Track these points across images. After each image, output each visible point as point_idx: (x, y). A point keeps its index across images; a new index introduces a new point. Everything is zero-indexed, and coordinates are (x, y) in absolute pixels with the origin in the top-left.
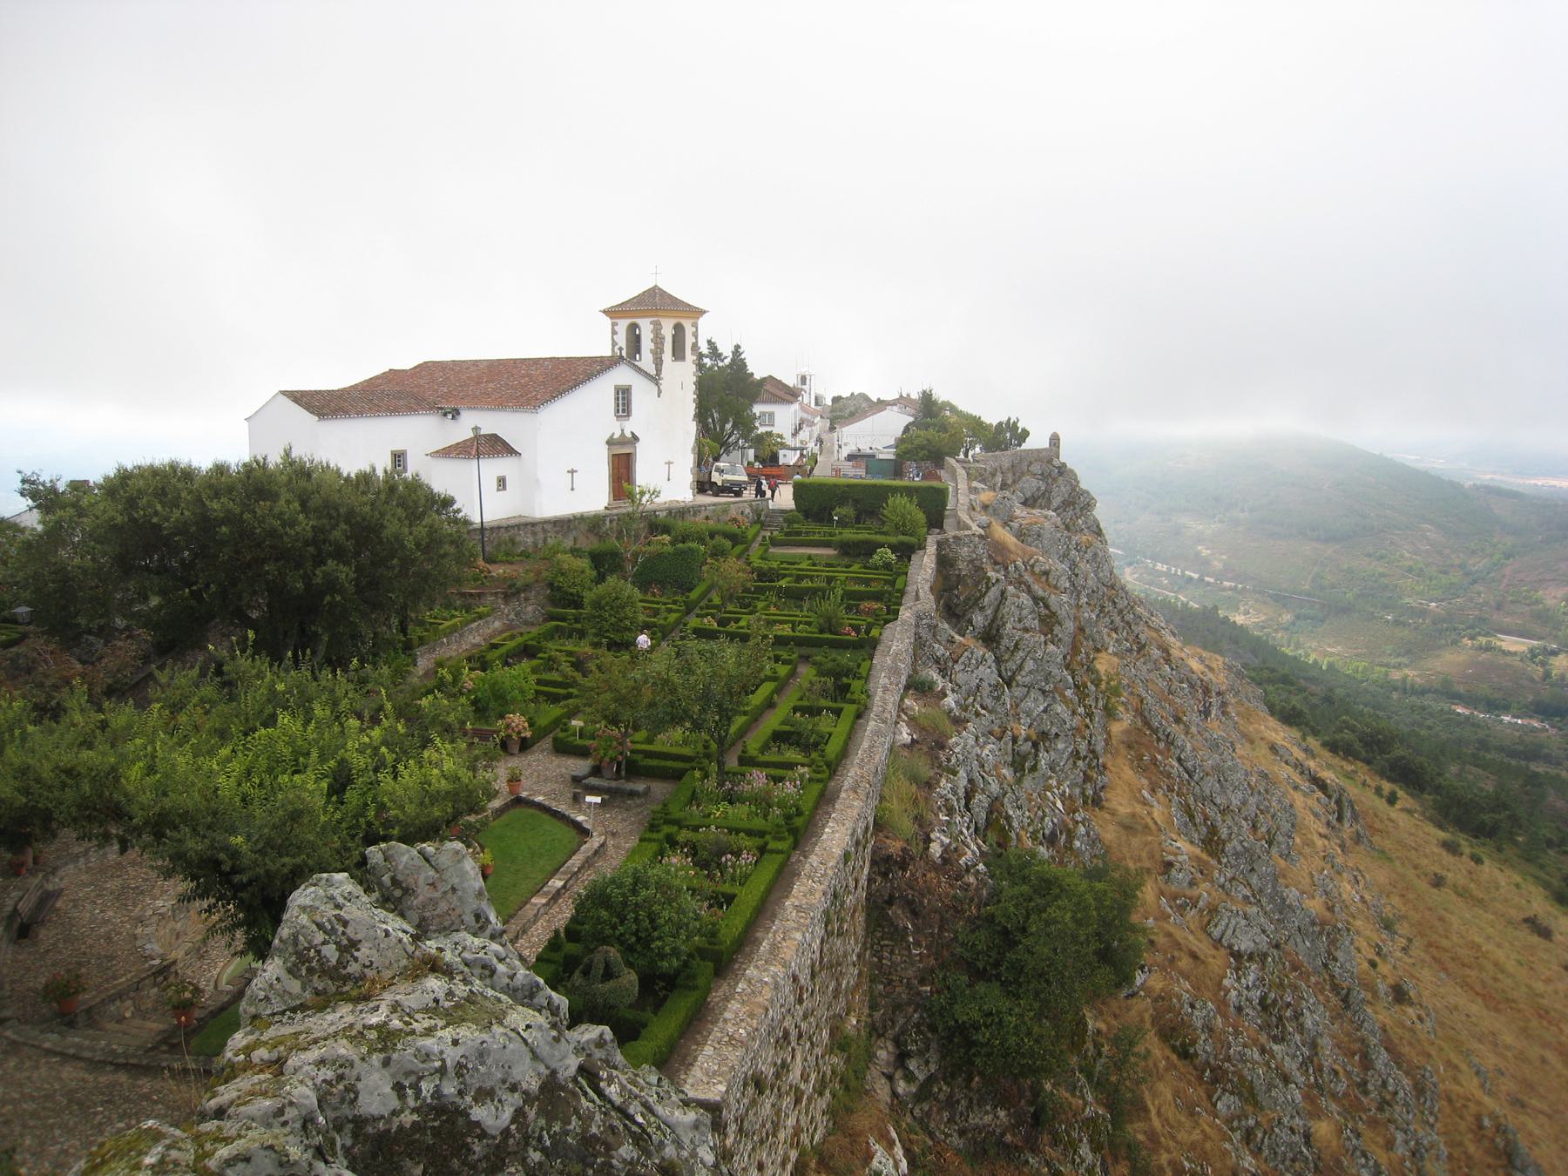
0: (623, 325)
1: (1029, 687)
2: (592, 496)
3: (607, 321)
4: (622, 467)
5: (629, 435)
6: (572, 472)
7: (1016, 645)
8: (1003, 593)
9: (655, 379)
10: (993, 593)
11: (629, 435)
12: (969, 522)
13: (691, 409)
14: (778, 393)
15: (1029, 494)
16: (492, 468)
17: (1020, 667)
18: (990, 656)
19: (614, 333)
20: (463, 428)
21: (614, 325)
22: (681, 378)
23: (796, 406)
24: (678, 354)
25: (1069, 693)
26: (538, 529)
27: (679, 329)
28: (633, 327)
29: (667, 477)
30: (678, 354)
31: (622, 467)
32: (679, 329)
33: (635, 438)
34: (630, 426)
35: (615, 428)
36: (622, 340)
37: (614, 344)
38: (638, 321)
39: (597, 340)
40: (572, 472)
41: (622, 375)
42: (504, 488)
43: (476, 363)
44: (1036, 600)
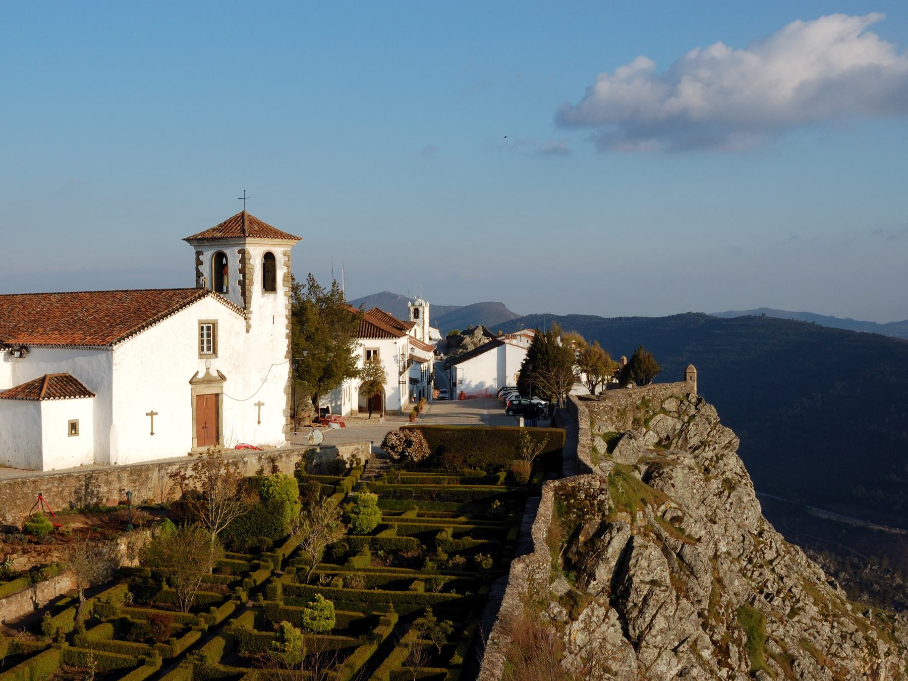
0: (208, 256)
1: (661, 649)
2: (176, 441)
3: (191, 250)
4: (208, 413)
5: (215, 374)
6: (259, 405)
7: (645, 600)
8: (631, 540)
9: (244, 309)
10: (617, 543)
11: (215, 374)
12: (592, 466)
13: (282, 345)
14: (384, 326)
15: (663, 435)
16: (55, 412)
17: (650, 626)
18: (614, 615)
19: (199, 263)
20: (40, 364)
21: (198, 254)
22: (272, 312)
23: (403, 341)
24: (269, 285)
25: (706, 654)
26: (113, 477)
27: (269, 258)
28: (220, 257)
29: (259, 419)
30: (269, 285)
31: (208, 413)
32: (269, 258)
33: (223, 378)
34: (217, 365)
35: (199, 367)
36: (207, 269)
37: (199, 275)
38: (227, 251)
39: (179, 266)
40: (152, 414)
41: (209, 307)
42: (76, 433)
43: (647, 318)
44: (666, 551)
